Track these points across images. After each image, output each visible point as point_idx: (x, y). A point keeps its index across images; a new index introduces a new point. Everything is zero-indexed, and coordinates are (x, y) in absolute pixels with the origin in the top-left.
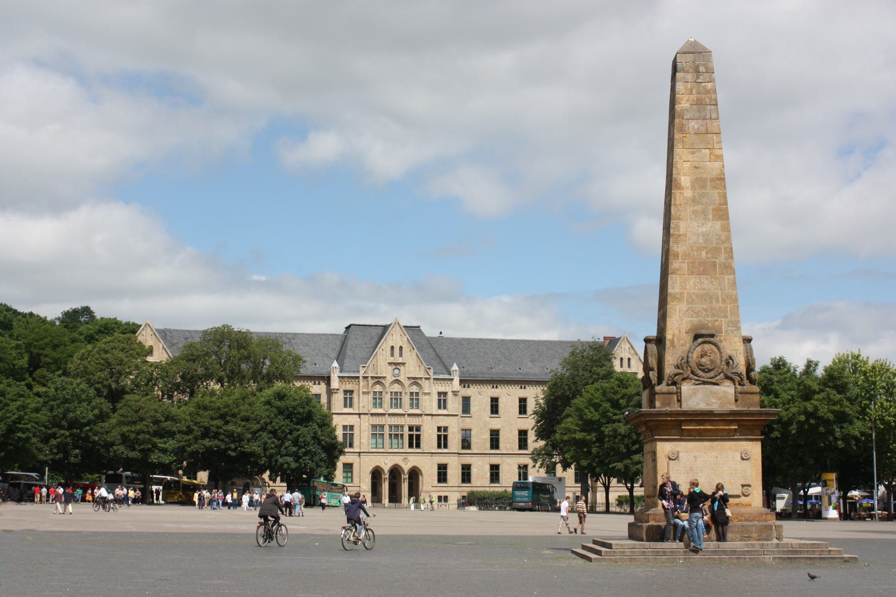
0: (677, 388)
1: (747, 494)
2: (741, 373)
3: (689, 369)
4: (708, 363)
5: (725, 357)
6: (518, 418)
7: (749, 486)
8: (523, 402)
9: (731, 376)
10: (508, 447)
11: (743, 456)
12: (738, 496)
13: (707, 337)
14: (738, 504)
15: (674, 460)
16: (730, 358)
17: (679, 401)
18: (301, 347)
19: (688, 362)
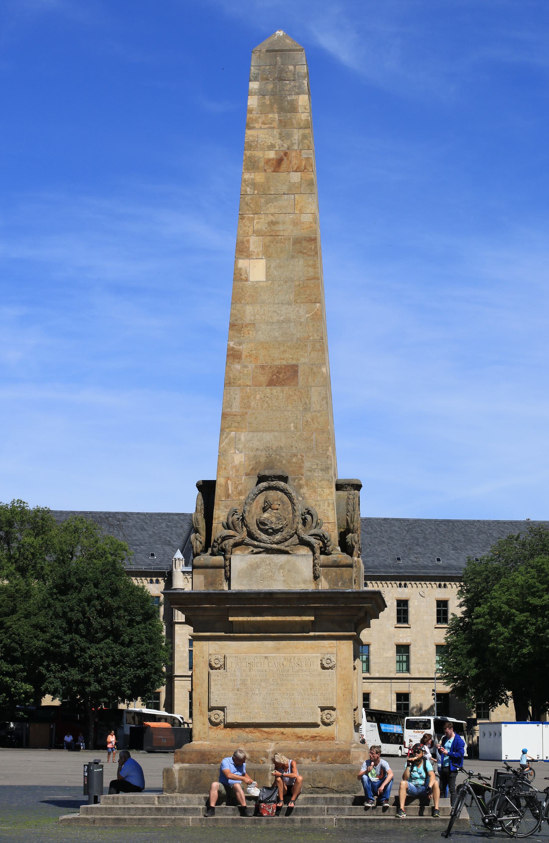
0: (225, 559)
1: (328, 721)
2: (323, 535)
3: (245, 529)
4: (274, 519)
5: (300, 509)
6: (435, 628)
7: (333, 709)
8: (442, 605)
9: (309, 540)
10: (421, 669)
11: (324, 663)
12: (315, 725)
13: (272, 481)
14: (316, 737)
15: (219, 668)
16: (309, 513)
17: (228, 579)
18: (134, 531)
19: (243, 519)
